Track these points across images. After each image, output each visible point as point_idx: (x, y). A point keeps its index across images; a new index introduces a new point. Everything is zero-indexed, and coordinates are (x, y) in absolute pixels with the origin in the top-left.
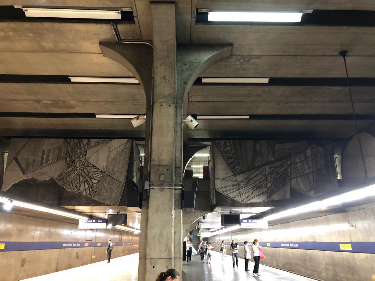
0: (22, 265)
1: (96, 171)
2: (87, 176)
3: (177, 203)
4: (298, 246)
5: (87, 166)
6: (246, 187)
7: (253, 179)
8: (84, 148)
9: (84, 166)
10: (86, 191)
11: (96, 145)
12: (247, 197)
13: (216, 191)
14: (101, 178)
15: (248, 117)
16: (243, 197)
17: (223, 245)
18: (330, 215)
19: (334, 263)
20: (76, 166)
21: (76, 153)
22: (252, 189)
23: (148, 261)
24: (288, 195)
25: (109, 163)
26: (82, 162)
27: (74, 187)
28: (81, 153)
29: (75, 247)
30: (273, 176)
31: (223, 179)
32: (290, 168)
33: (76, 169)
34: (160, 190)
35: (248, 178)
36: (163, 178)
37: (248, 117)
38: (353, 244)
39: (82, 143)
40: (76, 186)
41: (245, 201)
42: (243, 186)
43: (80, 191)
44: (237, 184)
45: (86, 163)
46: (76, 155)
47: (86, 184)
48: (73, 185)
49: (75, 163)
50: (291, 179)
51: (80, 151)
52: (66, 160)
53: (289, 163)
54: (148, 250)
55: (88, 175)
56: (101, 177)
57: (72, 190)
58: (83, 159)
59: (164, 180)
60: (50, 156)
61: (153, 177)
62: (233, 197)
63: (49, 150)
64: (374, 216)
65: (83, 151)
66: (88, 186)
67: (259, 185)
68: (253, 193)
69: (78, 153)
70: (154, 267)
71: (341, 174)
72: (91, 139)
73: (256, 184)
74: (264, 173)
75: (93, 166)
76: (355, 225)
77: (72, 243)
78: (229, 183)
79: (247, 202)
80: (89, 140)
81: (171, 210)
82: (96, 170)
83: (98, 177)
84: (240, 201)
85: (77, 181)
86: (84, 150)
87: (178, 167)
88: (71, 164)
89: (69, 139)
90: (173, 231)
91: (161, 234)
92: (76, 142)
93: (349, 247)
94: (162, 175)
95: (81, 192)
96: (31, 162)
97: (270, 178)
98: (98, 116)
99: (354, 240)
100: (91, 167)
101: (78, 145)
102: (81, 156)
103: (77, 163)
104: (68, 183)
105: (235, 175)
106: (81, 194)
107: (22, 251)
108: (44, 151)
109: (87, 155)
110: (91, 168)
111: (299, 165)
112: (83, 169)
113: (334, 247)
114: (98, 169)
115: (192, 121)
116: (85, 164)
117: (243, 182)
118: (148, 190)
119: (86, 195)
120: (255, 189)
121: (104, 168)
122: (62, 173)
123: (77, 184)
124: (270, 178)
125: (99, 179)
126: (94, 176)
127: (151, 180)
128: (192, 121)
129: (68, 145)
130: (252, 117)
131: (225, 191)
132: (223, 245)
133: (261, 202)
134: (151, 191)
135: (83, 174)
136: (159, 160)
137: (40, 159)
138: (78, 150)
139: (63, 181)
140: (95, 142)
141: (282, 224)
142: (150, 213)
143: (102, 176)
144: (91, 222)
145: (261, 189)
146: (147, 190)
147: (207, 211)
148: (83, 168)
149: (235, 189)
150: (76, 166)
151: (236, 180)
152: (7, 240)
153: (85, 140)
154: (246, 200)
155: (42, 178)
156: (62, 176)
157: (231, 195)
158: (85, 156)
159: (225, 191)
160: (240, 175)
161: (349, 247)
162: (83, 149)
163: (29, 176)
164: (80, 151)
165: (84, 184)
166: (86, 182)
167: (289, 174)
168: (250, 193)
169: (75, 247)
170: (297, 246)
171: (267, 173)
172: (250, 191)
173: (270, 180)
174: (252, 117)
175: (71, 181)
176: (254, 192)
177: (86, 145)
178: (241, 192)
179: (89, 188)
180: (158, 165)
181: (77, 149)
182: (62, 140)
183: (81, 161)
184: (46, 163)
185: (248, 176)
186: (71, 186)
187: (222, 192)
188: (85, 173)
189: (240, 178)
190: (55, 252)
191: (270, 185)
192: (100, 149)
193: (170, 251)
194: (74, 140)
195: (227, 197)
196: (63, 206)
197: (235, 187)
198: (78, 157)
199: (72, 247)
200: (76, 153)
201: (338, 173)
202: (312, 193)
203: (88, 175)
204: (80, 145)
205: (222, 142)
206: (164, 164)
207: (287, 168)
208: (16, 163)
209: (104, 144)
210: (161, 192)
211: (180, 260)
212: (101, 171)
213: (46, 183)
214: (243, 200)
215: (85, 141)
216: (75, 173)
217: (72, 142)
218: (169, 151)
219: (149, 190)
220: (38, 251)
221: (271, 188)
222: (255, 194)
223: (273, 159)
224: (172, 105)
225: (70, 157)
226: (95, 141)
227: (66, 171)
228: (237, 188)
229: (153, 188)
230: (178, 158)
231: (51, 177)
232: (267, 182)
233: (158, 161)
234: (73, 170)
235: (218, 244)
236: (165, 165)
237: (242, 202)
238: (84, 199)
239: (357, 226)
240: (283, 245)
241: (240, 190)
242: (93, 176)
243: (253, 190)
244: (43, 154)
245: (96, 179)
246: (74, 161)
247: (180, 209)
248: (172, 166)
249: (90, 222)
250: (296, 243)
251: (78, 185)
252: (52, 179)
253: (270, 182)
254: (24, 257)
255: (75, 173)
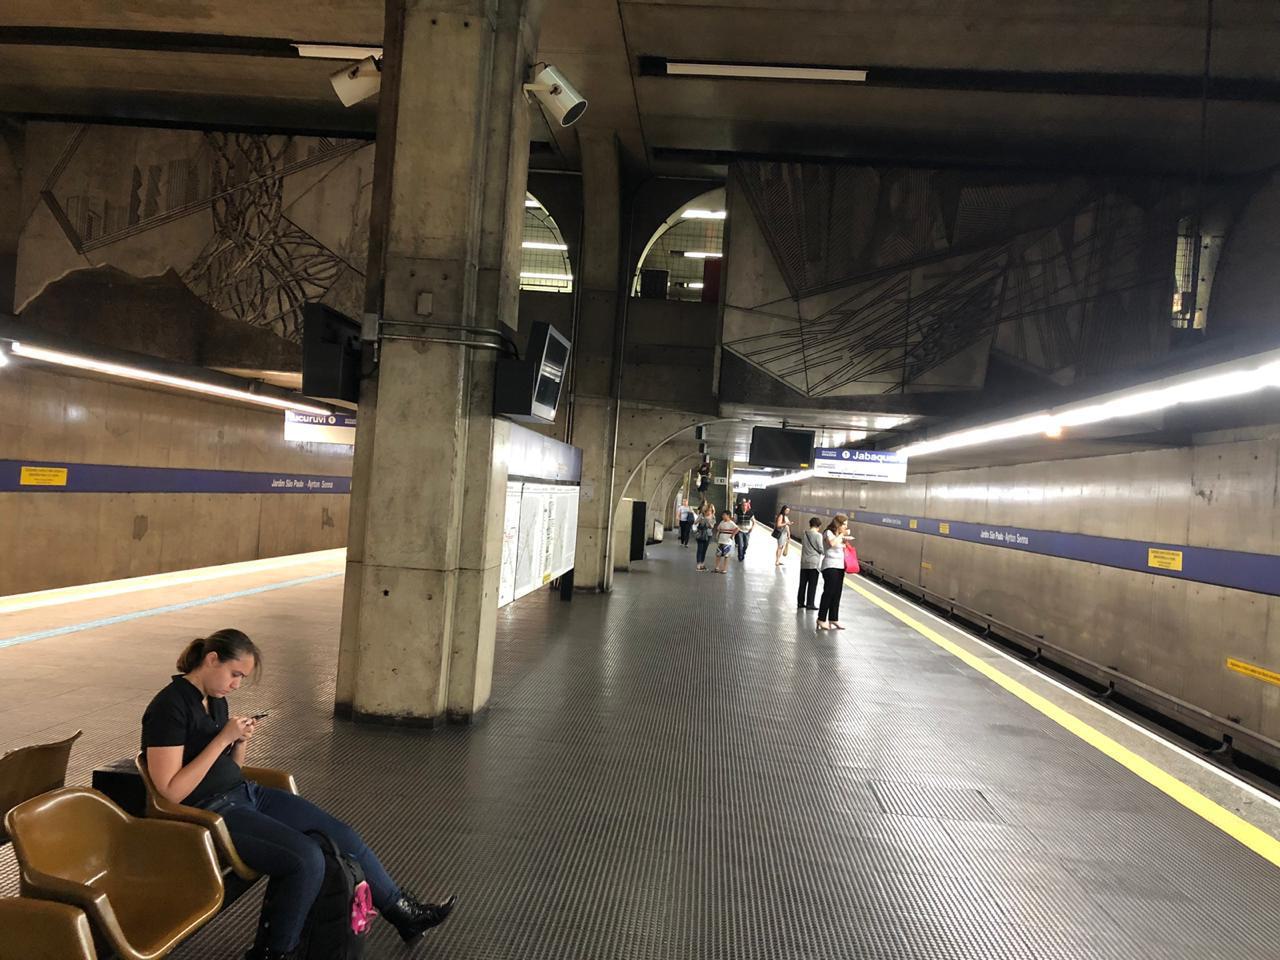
0: (138, 535)
1: (316, 256)
2: (287, 269)
3: (477, 394)
4: (1027, 543)
5: (284, 236)
6: (830, 340)
7: (860, 317)
8: (273, 170)
9: (275, 233)
10: (283, 320)
11: (316, 159)
12: (828, 378)
13: (722, 348)
14: (333, 279)
15: (860, 76)
16: (815, 376)
17: (783, 520)
18: (1144, 451)
19: (1122, 606)
20: (247, 234)
21: (245, 186)
22: (852, 349)
23: (369, 573)
24: (978, 380)
25: (357, 229)
26: (270, 222)
27: (246, 308)
28: (264, 188)
29: (314, 491)
30: (932, 307)
31: (751, 309)
32: (1000, 280)
33: (249, 244)
34: (416, 348)
35: (843, 309)
36: (426, 305)
37: (860, 76)
38: (1190, 552)
39: (268, 151)
40: (252, 304)
41: (818, 390)
42: (820, 336)
43: (266, 322)
44: (801, 328)
45: (283, 223)
46: (247, 194)
47: (284, 297)
48: (242, 297)
49: (243, 224)
50: (999, 320)
51: (261, 180)
52: (214, 209)
53: (1002, 260)
54: (370, 539)
55: (289, 266)
56: (332, 276)
57: (240, 313)
58: (270, 209)
59: (430, 314)
60: (160, 194)
61: (393, 300)
62: (779, 374)
63: (156, 171)
64: (1277, 466)
65: (270, 182)
66: (292, 306)
67: (877, 337)
68: (851, 363)
69: (252, 188)
70: (386, 593)
71: (1205, 311)
72: (297, 138)
73: (869, 331)
74: (903, 296)
75: (305, 238)
76: (1211, 492)
77: (305, 478)
78: (775, 325)
79: (827, 395)
80: (290, 138)
81: (450, 415)
82: (315, 250)
83: (323, 275)
84: (804, 389)
85: (254, 283)
86: (273, 177)
87: (488, 267)
88: (230, 224)
89: (220, 133)
90: (457, 486)
91: (414, 494)
92: (245, 147)
93: (1176, 562)
94: (424, 294)
95: (269, 323)
96: (100, 209)
97: (920, 314)
98: (305, 51)
99: (1198, 539)
100: (299, 240)
101: (253, 159)
102: (265, 199)
103: (251, 221)
104: (226, 289)
105: (796, 297)
106: (268, 331)
107: (131, 494)
108: (137, 172)
109: (284, 196)
110: (298, 244)
111: (1036, 271)
112: (272, 245)
113: (1129, 555)
114: (322, 247)
115: (555, 90)
116: (277, 226)
117: (822, 324)
118: (376, 345)
119: (285, 336)
120: (862, 348)
121: (340, 245)
122: (205, 254)
123: (256, 295)
124: (920, 314)
125: (326, 283)
126: (310, 271)
127: (385, 308)
128: (555, 90)
129: (220, 153)
130: (878, 75)
131: (754, 354)
132: (783, 520)
133: (875, 396)
134: (386, 349)
135: (274, 262)
136: (414, 238)
137: (126, 200)
138: (254, 176)
139: (209, 284)
140: (311, 151)
141: (994, 466)
142: (381, 423)
143: (337, 272)
144: (322, 424)
145: (885, 350)
146: (371, 343)
147: (704, 413)
148: (272, 241)
149: (793, 344)
150: (250, 233)
151: (797, 317)
152: (74, 459)
153: (274, 138)
154: (824, 386)
155: (141, 270)
156: (206, 267)
157: (775, 368)
158: (277, 200)
159: (754, 354)
160: (815, 299)
161: (1176, 562)
162: (269, 172)
163: (97, 259)
164: (261, 180)
165: (276, 297)
166: (282, 292)
167: (995, 303)
168: (844, 362)
169: (314, 491)
170: (1024, 540)
171: (912, 296)
172: (840, 358)
173: (922, 322)
174: (878, 75)
175: (234, 284)
176: (855, 361)
177: (277, 158)
178: (809, 358)
179: (294, 312)
180: (413, 259)
181: (251, 172)
182: (195, 136)
183: (265, 216)
184: (147, 216)
185: (846, 303)
186: (235, 300)
187: (744, 355)
188: (280, 261)
189: (812, 308)
190: (248, 501)
191: (917, 338)
192: (326, 176)
193: (440, 549)
194: (237, 137)
195: (758, 375)
196: (210, 365)
197: (789, 340)
198: (253, 202)
199: (306, 490)
200: (245, 186)
201: (1198, 306)
202: (1066, 375)
203: (289, 266)
204: (260, 158)
205: (765, 171)
206: (434, 253)
207: (993, 280)
208: (50, 211)
209: (341, 158)
210: (419, 355)
211: (476, 577)
212: (332, 257)
213: (153, 287)
214: (816, 386)
215: (276, 143)
216: (248, 259)
217: (233, 144)
218: (454, 208)
219: (380, 341)
220: (189, 496)
221: (921, 352)
222: (859, 367)
223: (943, 244)
224: (473, 21)
225: (229, 202)
226: (310, 147)
227: (217, 248)
228: (798, 343)
229: (392, 340)
230: (491, 233)
231: (168, 268)
232: (910, 328)
233: (413, 241)
234: (240, 248)
235: (805, 509)
236: (436, 257)
237: (811, 394)
238: (280, 348)
239: (1215, 496)
240: (985, 535)
241: (806, 353)
242: (305, 270)
243: (853, 353)
244: (138, 184)
245: (316, 281)
246: (242, 213)
247: (489, 415)
248: (461, 263)
249: (319, 423)
250: (1022, 532)
251: (257, 301)
252: (172, 273)
253: (919, 329)
254: (140, 511)
255: (248, 259)
